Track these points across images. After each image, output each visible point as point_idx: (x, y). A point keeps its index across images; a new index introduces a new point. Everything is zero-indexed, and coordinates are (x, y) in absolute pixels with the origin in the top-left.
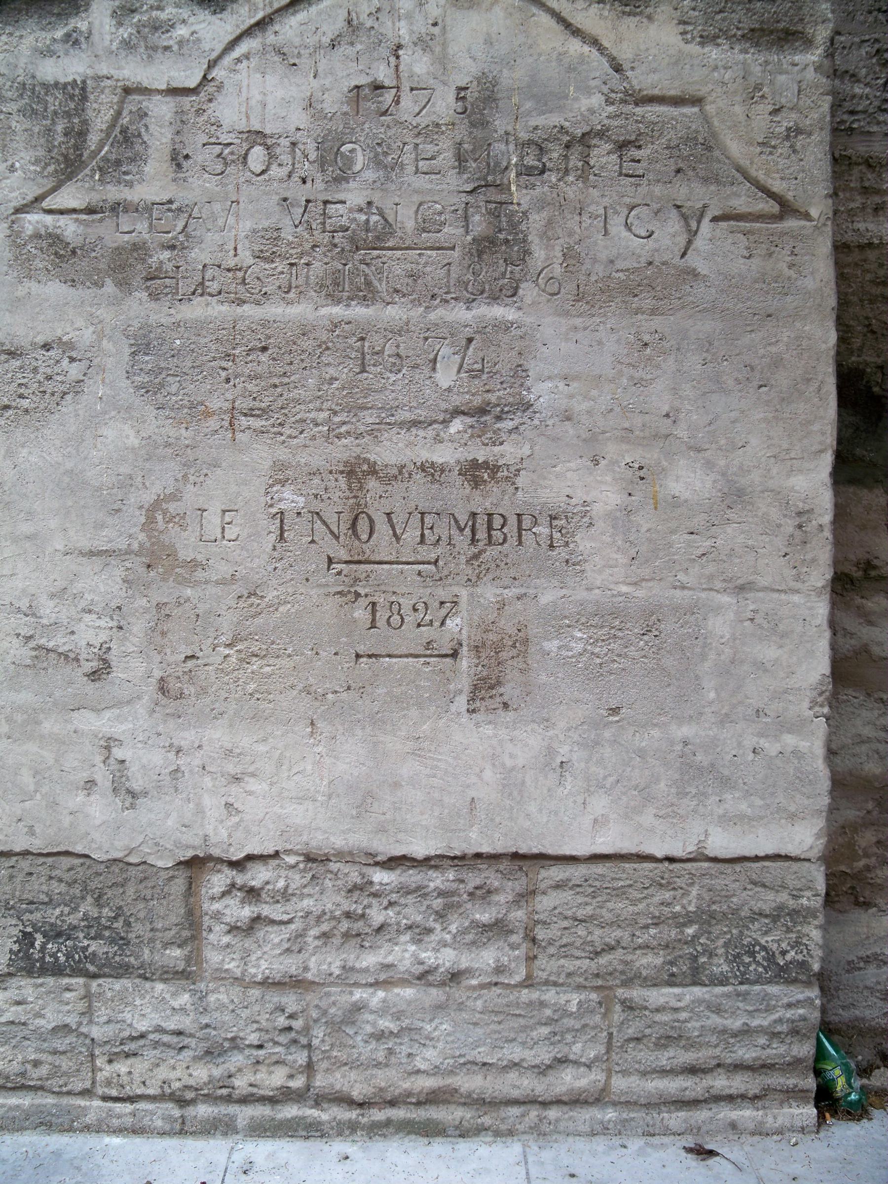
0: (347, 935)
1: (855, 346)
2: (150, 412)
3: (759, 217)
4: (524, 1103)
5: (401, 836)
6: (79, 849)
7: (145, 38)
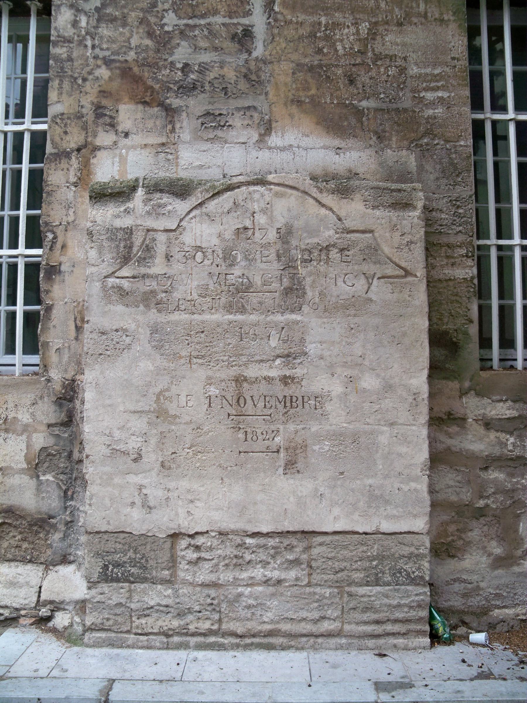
0: (235, 565)
1: (445, 322)
2: (158, 356)
3: (397, 277)
4: (308, 636)
5: (257, 524)
6: (128, 530)
7: (155, 210)
